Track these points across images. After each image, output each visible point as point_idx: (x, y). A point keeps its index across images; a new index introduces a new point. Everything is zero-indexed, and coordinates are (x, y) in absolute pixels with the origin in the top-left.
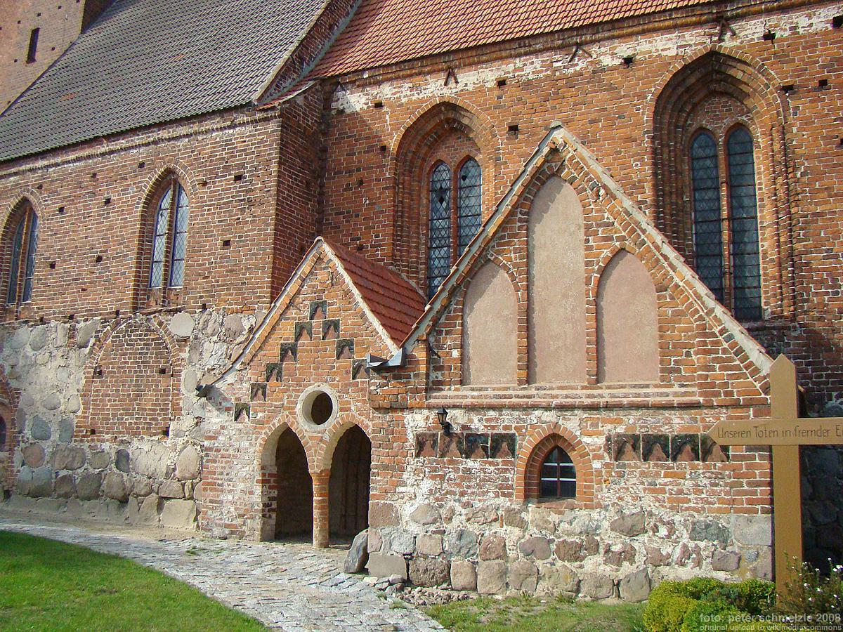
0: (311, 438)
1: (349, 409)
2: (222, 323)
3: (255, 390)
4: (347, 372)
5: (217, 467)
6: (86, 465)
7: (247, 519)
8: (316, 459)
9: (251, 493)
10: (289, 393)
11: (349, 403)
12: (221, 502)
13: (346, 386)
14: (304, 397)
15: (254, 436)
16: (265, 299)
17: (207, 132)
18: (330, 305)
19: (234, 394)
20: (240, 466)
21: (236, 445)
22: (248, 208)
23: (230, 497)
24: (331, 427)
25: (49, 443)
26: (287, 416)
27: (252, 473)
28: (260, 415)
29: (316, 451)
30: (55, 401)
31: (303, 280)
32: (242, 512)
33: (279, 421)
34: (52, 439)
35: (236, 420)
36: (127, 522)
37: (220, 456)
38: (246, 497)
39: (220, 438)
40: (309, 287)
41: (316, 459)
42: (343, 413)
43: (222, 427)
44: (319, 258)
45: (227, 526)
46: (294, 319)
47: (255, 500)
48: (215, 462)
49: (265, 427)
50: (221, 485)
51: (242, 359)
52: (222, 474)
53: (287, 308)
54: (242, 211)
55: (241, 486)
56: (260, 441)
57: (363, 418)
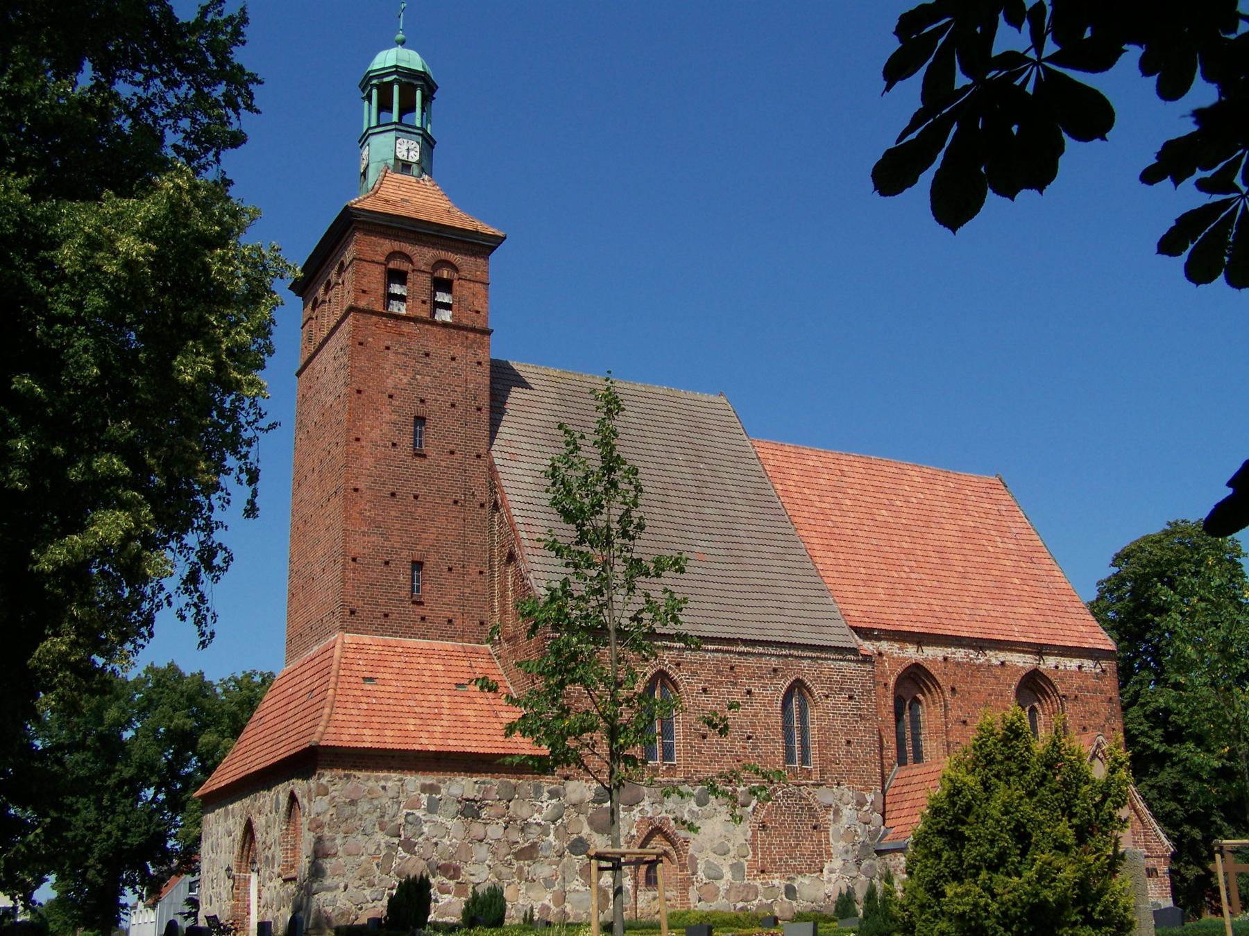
6: (759, 898)
17: (826, 659)
25: (723, 882)
30: (725, 849)
34: (725, 878)
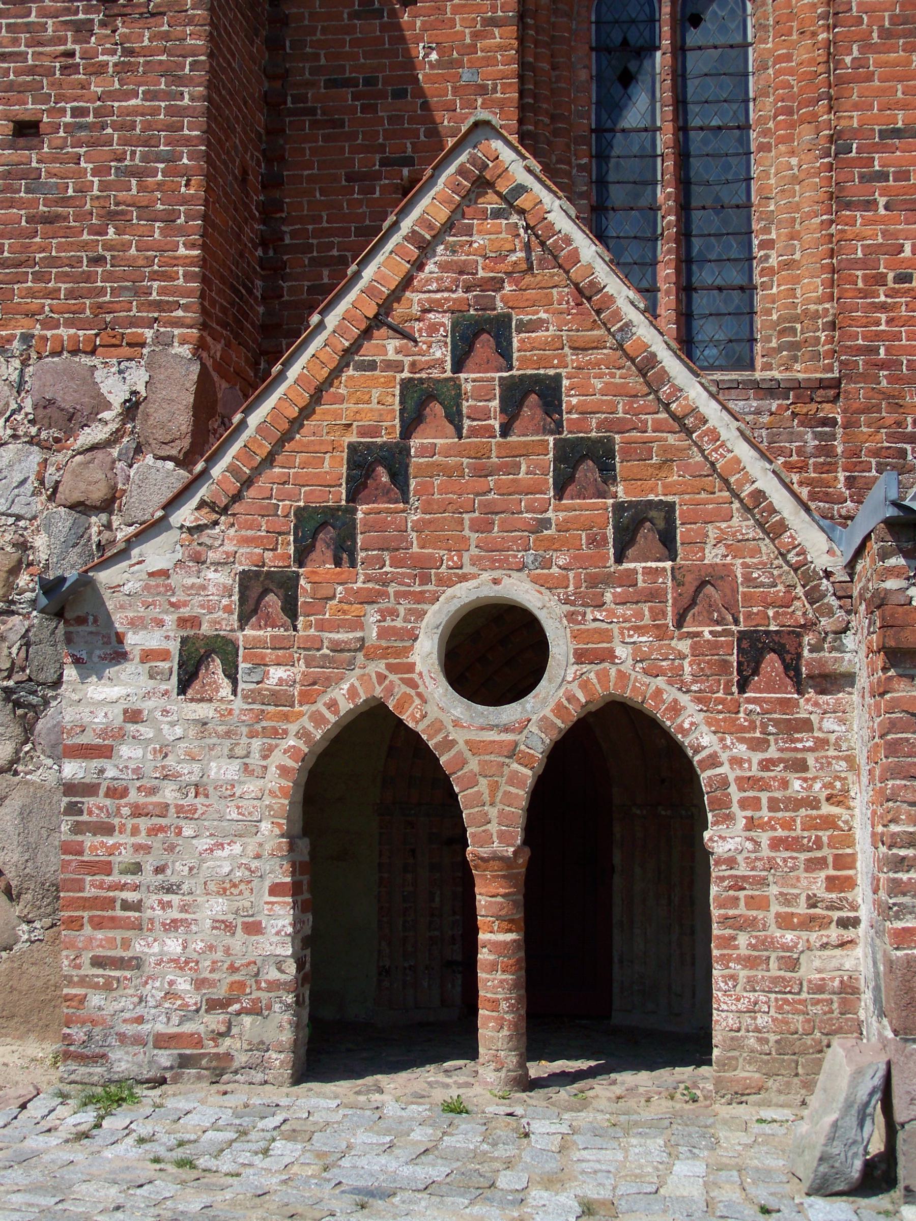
0: (475, 747)
1: (610, 656)
2: (21, 382)
3: (254, 594)
4: (592, 540)
5: (116, 846)
7: (238, 1013)
8: (493, 812)
9: (253, 928)
10: (384, 604)
11: (606, 636)
12: (136, 964)
13: (594, 581)
14: (443, 619)
15: (256, 744)
16: (180, 313)
18: (525, 327)
19: (172, 605)
20: (203, 843)
21: (189, 772)
22: (103, 24)
23: (173, 946)
24: (547, 712)
26: (381, 678)
27: (254, 864)
28: (277, 674)
29: (494, 788)
31: (425, 248)
32: (221, 992)
33: (352, 693)
35: (183, 688)
36: (324, 1174)
37: (126, 811)
38: (238, 941)
39: (125, 751)
40: (444, 267)
41: (493, 812)
42: (585, 668)
43: (133, 716)
44: (481, 177)
45: (162, 1041)
46: (397, 366)
47: (269, 949)
48: (108, 830)
49: (301, 714)
50: (137, 906)
51: (203, 492)
52: (136, 868)
53: (367, 334)
54: (83, 30)
55: (218, 907)
56: (279, 758)
57: (660, 682)
